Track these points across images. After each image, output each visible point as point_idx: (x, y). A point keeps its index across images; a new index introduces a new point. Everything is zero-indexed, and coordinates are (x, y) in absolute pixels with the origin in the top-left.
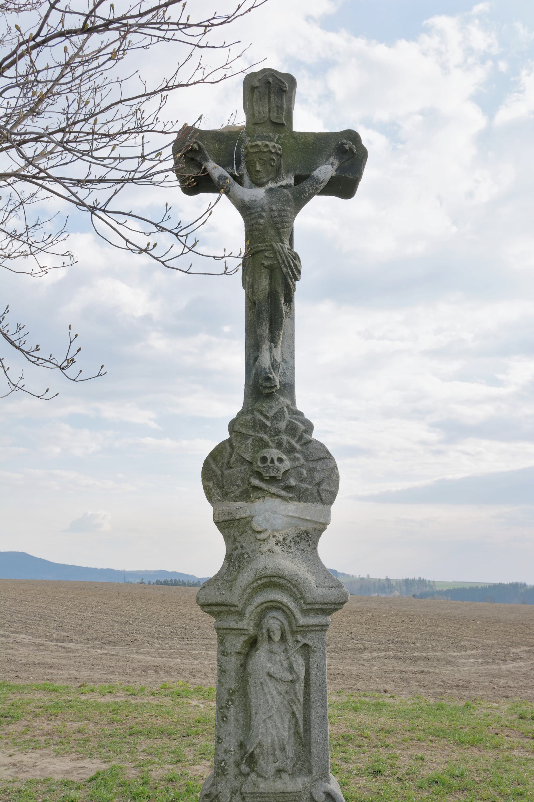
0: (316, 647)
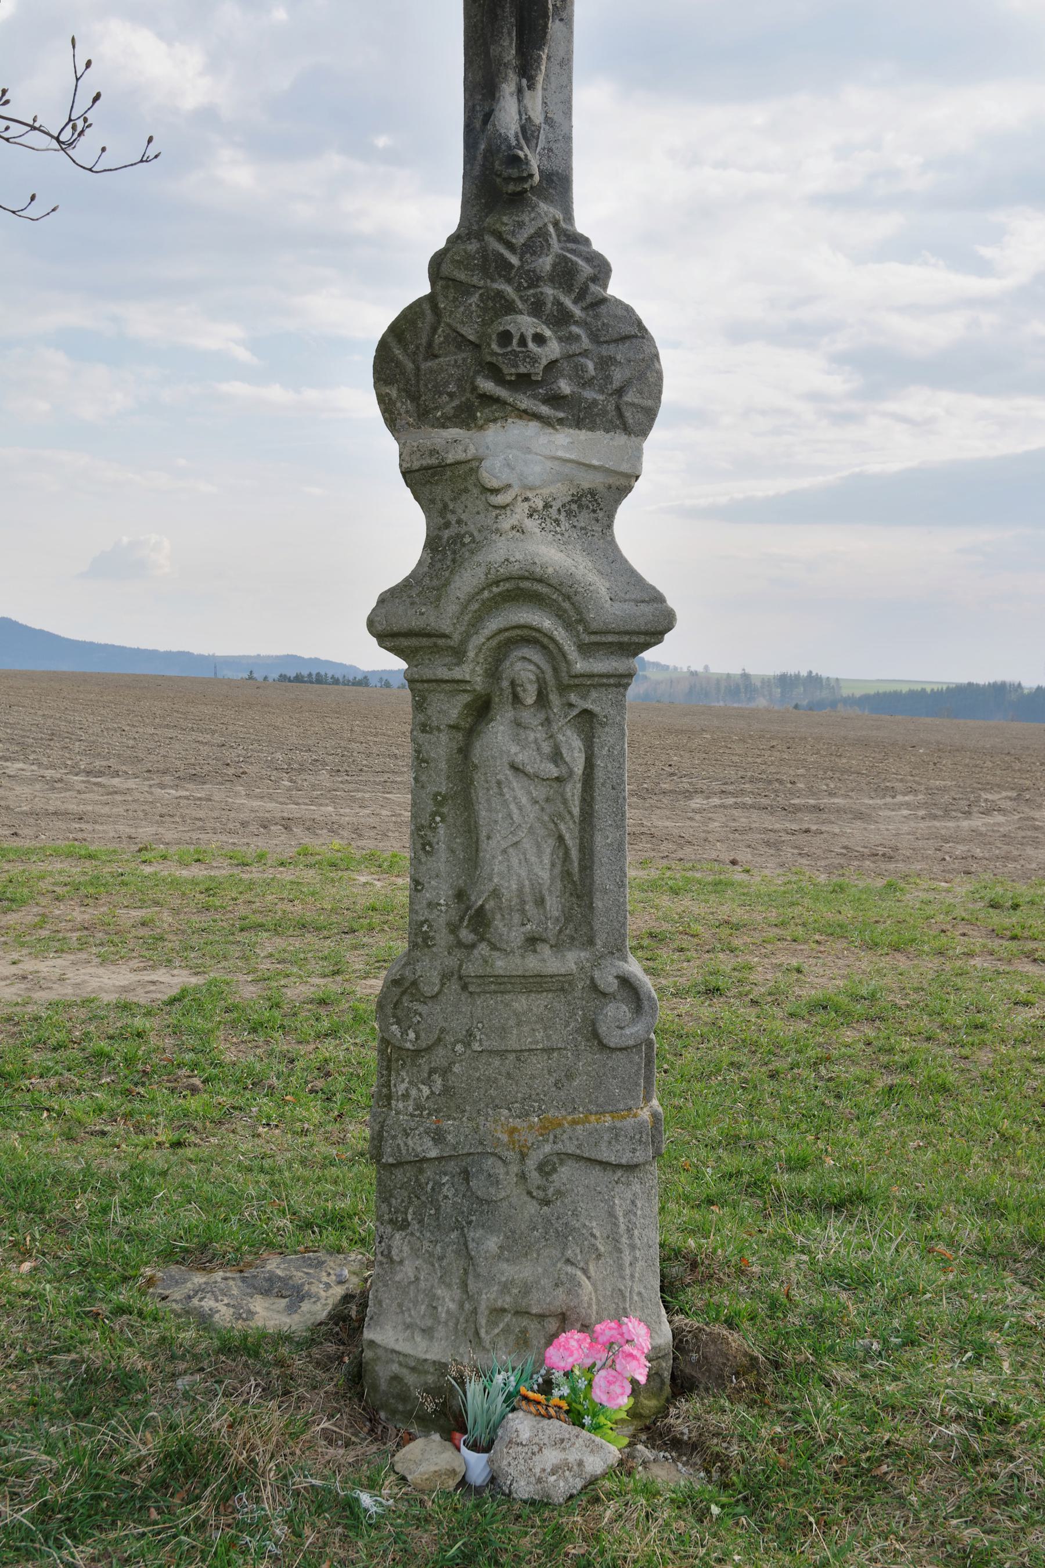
0: (605, 717)
